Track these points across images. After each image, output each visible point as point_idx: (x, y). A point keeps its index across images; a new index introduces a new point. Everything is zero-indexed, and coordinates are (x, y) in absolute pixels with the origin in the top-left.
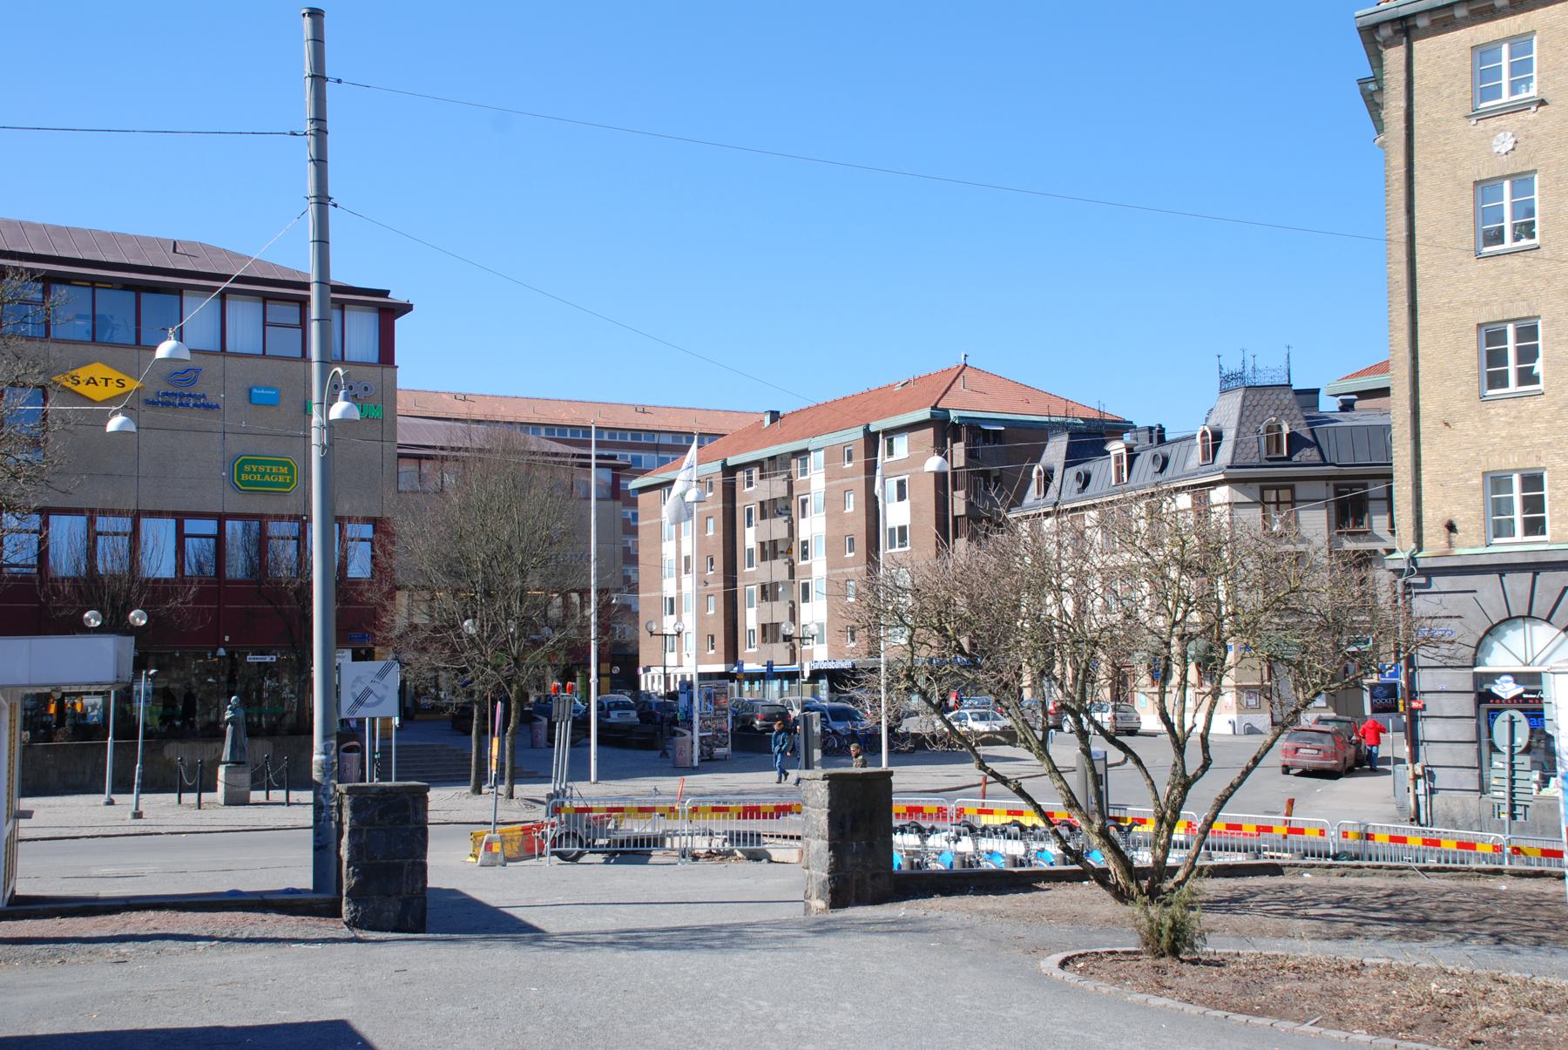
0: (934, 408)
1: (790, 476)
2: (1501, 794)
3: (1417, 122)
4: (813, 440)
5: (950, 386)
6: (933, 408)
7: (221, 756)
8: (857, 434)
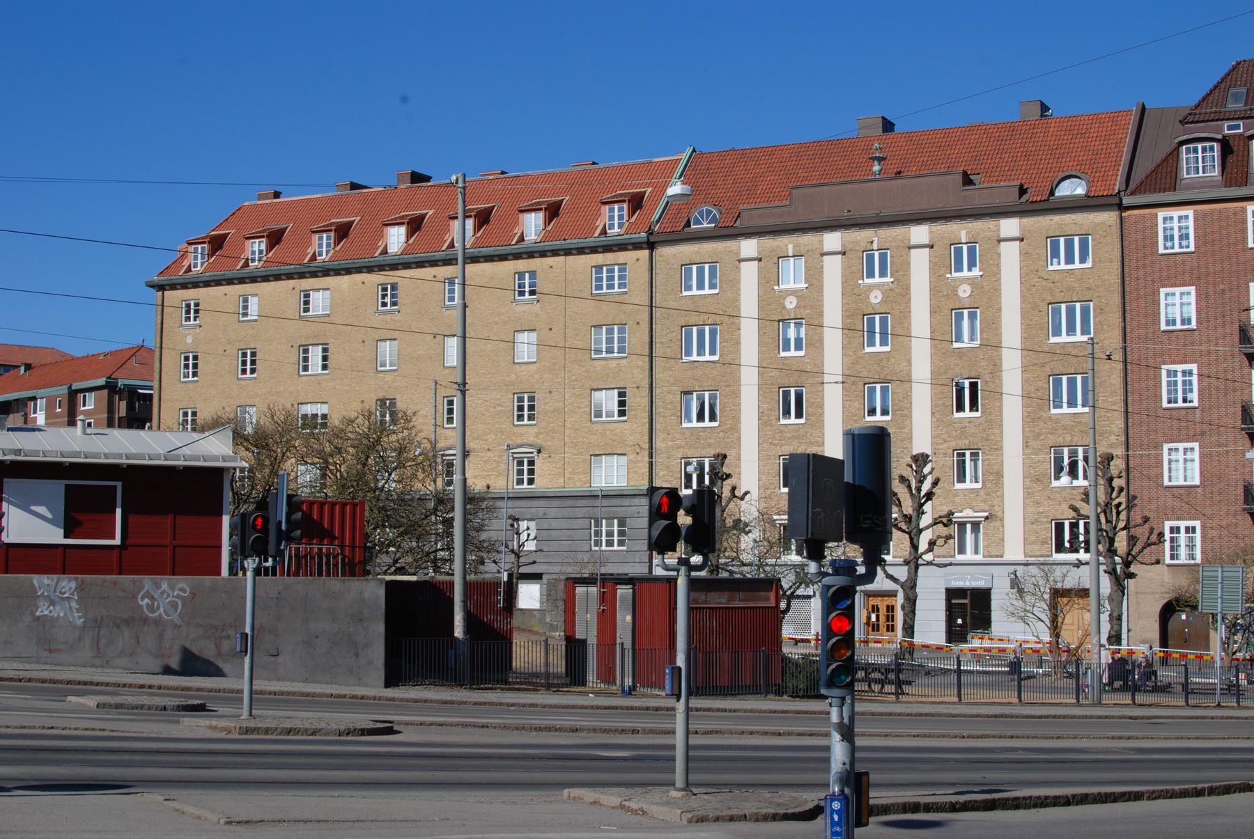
0: (107, 378)
1: (26, 414)
2: (1183, 552)
3: (164, 326)
4: (40, 391)
5: (126, 361)
6: (107, 378)
7: (1024, 254)
8: (63, 390)
